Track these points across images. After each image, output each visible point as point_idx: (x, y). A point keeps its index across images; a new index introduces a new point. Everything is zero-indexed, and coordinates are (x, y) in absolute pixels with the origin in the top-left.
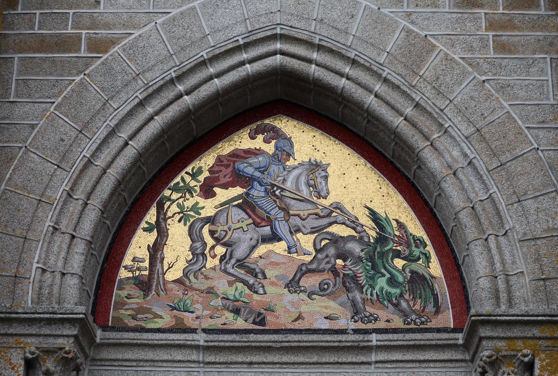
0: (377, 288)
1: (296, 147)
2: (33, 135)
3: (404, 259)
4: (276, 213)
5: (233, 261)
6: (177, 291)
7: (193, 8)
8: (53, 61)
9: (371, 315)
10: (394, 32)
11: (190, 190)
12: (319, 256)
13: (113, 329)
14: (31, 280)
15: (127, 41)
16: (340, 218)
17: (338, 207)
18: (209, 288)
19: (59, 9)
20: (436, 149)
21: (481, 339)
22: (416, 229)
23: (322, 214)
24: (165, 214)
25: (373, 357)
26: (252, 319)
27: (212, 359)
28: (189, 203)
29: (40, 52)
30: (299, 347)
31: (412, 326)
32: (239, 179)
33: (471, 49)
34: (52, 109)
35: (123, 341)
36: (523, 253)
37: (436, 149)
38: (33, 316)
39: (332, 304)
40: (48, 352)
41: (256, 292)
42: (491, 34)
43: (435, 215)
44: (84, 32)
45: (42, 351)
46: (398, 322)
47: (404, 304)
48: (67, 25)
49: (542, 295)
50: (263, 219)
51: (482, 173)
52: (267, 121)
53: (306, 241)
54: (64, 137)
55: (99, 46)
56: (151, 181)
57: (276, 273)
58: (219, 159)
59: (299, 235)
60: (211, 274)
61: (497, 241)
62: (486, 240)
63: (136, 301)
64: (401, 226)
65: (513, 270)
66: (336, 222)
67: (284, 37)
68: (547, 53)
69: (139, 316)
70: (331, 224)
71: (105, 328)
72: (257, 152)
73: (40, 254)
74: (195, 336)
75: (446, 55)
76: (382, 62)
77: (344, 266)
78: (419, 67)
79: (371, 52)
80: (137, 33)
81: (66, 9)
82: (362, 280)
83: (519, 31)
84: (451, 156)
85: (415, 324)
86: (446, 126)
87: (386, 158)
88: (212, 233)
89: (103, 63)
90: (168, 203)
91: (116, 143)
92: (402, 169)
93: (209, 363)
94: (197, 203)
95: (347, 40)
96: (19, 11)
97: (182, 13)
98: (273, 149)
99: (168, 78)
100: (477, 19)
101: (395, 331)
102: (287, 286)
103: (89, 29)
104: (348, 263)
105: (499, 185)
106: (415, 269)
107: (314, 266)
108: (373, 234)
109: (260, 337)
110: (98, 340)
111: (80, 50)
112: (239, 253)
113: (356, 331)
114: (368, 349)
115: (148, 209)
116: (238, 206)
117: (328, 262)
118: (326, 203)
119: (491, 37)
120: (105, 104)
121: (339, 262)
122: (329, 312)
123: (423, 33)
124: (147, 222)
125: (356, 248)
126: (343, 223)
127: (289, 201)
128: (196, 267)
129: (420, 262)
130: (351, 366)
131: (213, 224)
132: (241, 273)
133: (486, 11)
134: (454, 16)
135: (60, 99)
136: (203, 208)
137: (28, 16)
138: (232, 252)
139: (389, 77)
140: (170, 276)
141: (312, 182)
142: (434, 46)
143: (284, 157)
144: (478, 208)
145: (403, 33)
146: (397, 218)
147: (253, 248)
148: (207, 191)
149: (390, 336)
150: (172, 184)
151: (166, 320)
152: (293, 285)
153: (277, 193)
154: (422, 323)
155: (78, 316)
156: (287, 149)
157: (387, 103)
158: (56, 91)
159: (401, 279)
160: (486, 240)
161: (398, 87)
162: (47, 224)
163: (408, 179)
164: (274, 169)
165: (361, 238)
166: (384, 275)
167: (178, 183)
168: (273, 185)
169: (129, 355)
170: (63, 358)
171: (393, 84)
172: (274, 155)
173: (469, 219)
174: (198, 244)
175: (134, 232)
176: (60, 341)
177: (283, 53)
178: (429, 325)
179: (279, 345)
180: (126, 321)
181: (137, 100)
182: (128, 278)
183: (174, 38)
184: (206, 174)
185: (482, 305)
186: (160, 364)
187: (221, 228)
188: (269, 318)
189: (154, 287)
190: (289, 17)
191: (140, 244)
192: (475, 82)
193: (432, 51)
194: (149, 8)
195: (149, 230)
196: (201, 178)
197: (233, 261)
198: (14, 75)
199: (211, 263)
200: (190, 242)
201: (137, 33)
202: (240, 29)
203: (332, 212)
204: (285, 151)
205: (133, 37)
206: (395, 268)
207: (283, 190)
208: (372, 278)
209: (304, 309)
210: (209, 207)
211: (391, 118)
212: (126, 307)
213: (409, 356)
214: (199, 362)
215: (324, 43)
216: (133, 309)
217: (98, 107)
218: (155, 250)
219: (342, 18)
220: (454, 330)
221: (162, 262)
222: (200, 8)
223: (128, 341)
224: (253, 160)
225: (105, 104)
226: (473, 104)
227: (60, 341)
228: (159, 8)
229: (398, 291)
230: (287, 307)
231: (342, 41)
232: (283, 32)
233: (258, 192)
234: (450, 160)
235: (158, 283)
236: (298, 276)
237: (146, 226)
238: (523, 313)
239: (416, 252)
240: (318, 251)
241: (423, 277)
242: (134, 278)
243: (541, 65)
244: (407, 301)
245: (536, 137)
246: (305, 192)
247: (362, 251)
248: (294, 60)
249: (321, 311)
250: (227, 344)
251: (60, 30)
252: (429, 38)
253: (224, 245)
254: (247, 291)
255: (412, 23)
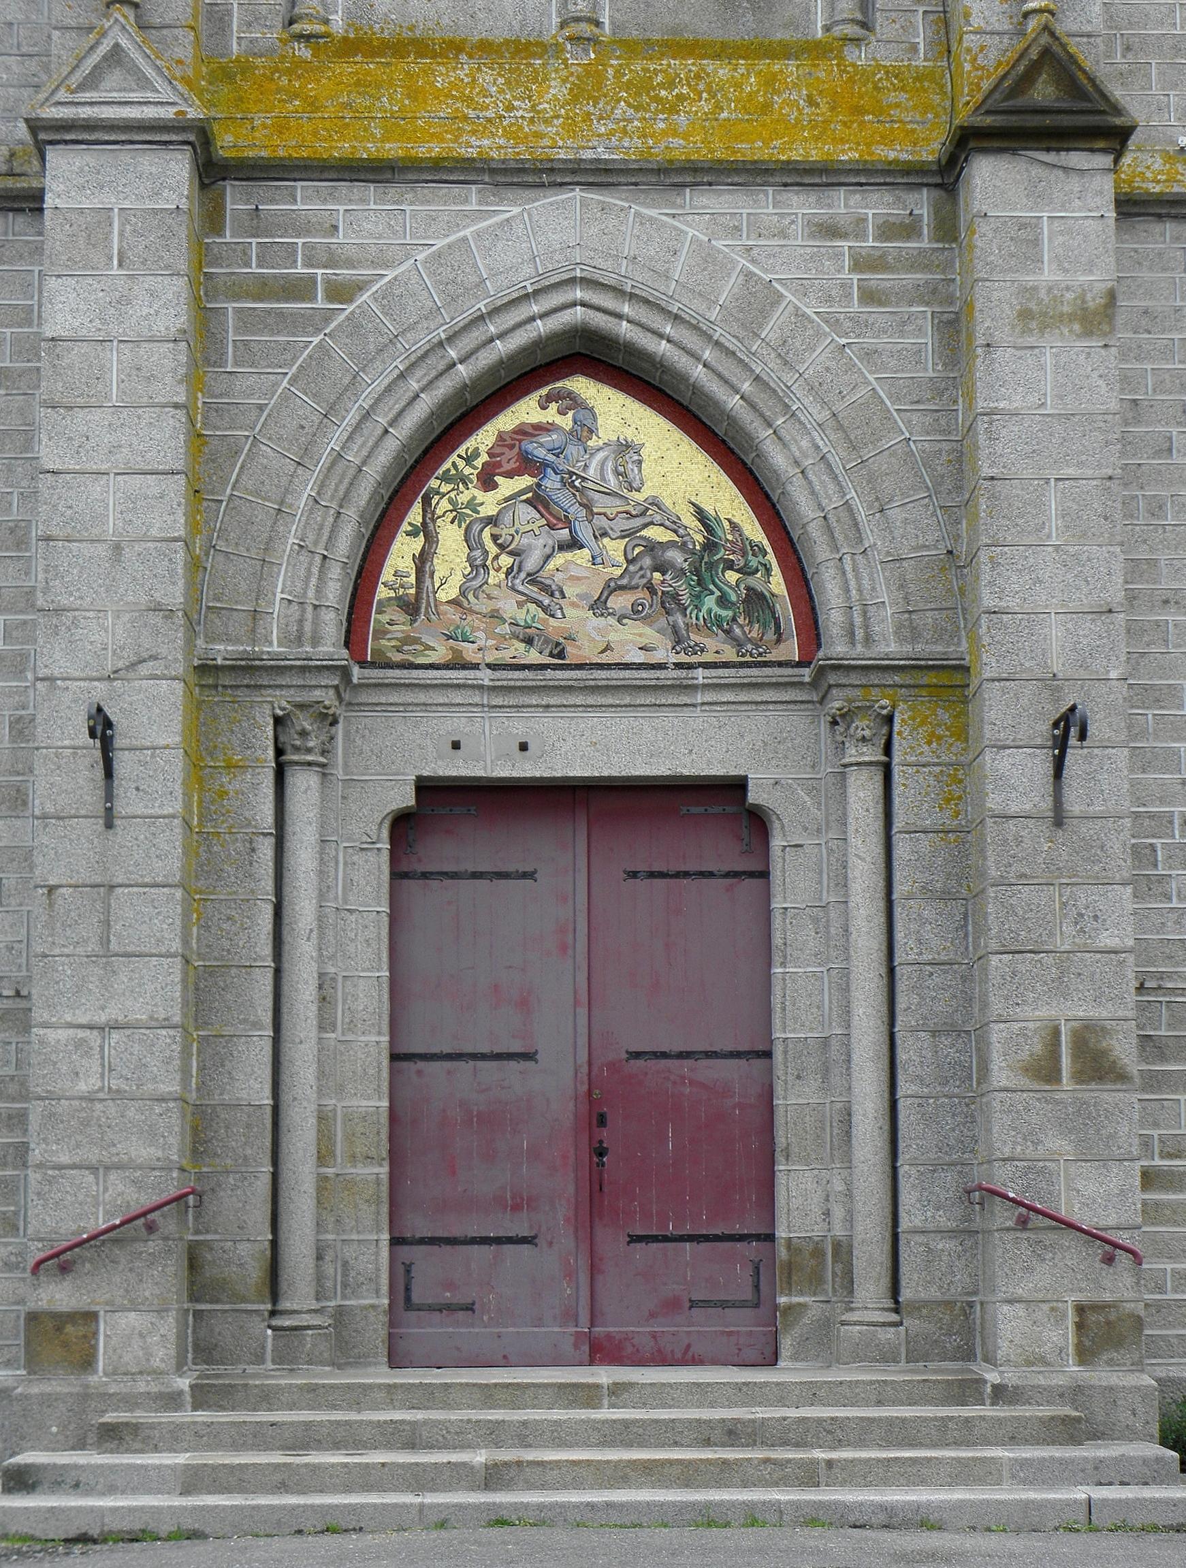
0: (704, 609)
1: (600, 421)
2: (262, 419)
3: (738, 571)
4: (577, 512)
5: (523, 575)
6: (452, 614)
7: (465, 239)
8: (280, 314)
9: (696, 645)
10: (729, 275)
11: (464, 480)
12: (632, 568)
13: (373, 665)
14: (275, 616)
15: (378, 286)
16: (658, 518)
17: (655, 503)
18: (493, 610)
19: (281, 237)
20: (780, 438)
21: (830, 686)
22: (754, 531)
23: (634, 513)
24: (433, 513)
25: (699, 699)
26: (548, 651)
27: (498, 701)
28: (464, 498)
29: (262, 301)
30: (607, 687)
31: (748, 658)
32: (527, 465)
33: (829, 300)
34: (285, 384)
35: (386, 681)
36: (885, 578)
37: (780, 438)
38: (282, 663)
39: (648, 631)
40: (301, 706)
41: (553, 616)
42: (855, 277)
43: (778, 513)
44: (320, 271)
45: (295, 706)
46: (730, 654)
47: (737, 631)
48: (296, 261)
49: (906, 632)
50: (559, 519)
51: (837, 472)
52: (559, 384)
53: (615, 549)
54: (303, 423)
55: (341, 292)
56: (413, 467)
57: (578, 591)
58: (501, 437)
59: (606, 540)
60: (495, 593)
61: (853, 560)
62: (840, 559)
63: (400, 630)
64: (734, 527)
65: (873, 598)
66: (652, 523)
67: (587, 282)
68: (927, 304)
69: (405, 648)
70: (646, 526)
71: (363, 664)
72: (549, 427)
73: (284, 581)
74: (478, 674)
75: (797, 308)
76: (712, 319)
77: (663, 582)
78: (761, 326)
79: (698, 305)
80: (390, 274)
81: (292, 237)
82: (685, 599)
83: (893, 273)
84: (800, 448)
85: (751, 655)
86: (794, 408)
87: (717, 435)
88: (495, 538)
89: (348, 318)
90: (437, 497)
91: (372, 430)
92: (737, 450)
93: (496, 706)
94: (474, 498)
95: (668, 287)
96: (228, 240)
97: (449, 246)
98: (571, 423)
99: (435, 341)
100: (838, 256)
101: (726, 665)
102: (591, 608)
103: (326, 267)
104: (668, 577)
105: (858, 489)
106: (752, 586)
107: (624, 582)
108: (699, 538)
109: (559, 674)
110: (355, 681)
111: (315, 298)
112: (531, 564)
113: (679, 666)
114: (694, 688)
115: (410, 504)
116: (527, 501)
117: (643, 576)
118: (639, 497)
119: (855, 282)
120: (355, 377)
121: (657, 575)
122: (644, 641)
123: (767, 277)
124: (410, 524)
125: (676, 556)
126: (661, 525)
127: (591, 493)
128: (476, 583)
129: (759, 575)
130: (671, 709)
131: (495, 525)
132: (533, 591)
133: (851, 244)
134: (808, 250)
135: (295, 368)
136: (482, 504)
137: (241, 246)
138: (521, 563)
139: (722, 340)
140: (442, 596)
141: (621, 469)
142: (782, 295)
143: (585, 434)
144: (832, 519)
145: (741, 277)
146: (729, 517)
147: (548, 557)
148: (487, 482)
149: (720, 672)
150: (440, 471)
151: (440, 653)
152: (599, 606)
153: (577, 483)
154: (760, 654)
155: (339, 663)
156: (588, 423)
157: (720, 376)
158: (288, 356)
159: (734, 598)
160: (840, 559)
161: (734, 353)
162: (290, 541)
163: (744, 464)
164: (573, 450)
165: (684, 544)
166: (712, 593)
167: (449, 470)
168: (571, 474)
169: (394, 697)
170: (321, 713)
171: (727, 349)
172: (571, 433)
173: (819, 533)
174: (478, 553)
175: (393, 537)
176: (317, 692)
177: (584, 304)
178: (768, 658)
179: (582, 684)
180: (389, 654)
181: (397, 372)
182: (390, 599)
183: (441, 283)
184: (484, 458)
185: (836, 647)
186: (434, 708)
187: (505, 531)
188: (569, 650)
189: (423, 610)
190: (592, 254)
191: (402, 552)
192: (833, 345)
193: (778, 302)
194: (405, 237)
195: (413, 534)
196: (479, 463)
197: (523, 575)
198: (230, 334)
199: (495, 578)
200: (467, 550)
201: (390, 274)
202: (528, 270)
203: (648, 509)
204: (585, 428)
205: (386, 279)
206: (727, 584)
207: (584, 479)
208: (698, 597)
209: (612, 637)
210: (489, 503)
211: (725, 398)
212: (388, 636)
213: (743, 697)
214: (483, 705)
215: (638, 292)
216: (397, 639)
217: (346, 381)
218: (423, 561)
219: (661, 254)
220: (799, 664)
221: (432, 577)
222: (474, 238)
223: (393, 681)
224: (544, 439)
225: (355, 377)
226: (829, 377)
227: (317, 694)
228: (418, 238)
229: (730, 613)
230: (591, 635)
231: (662, 289)
232: (584, 274)
233: (551, 483)
234: (797, 454)
235: (428, 604)
236: (605, 594)
237: (410, 528)
238: (882, 656)
239: (754, 563)
240: (630, 562)
241: (761, 596)
242: (398, 598)
243: (920, 322)
244: (741, 626)
245: (908, 423)
246: (612, 482)
247: (686, 561)
248: (599, 314)
249: (634, 640)
250: (518, 684)
251: (286, 268)
252: (774, 283)
253: (511, 553)
254: (542, 615)
255: (753, 261)
